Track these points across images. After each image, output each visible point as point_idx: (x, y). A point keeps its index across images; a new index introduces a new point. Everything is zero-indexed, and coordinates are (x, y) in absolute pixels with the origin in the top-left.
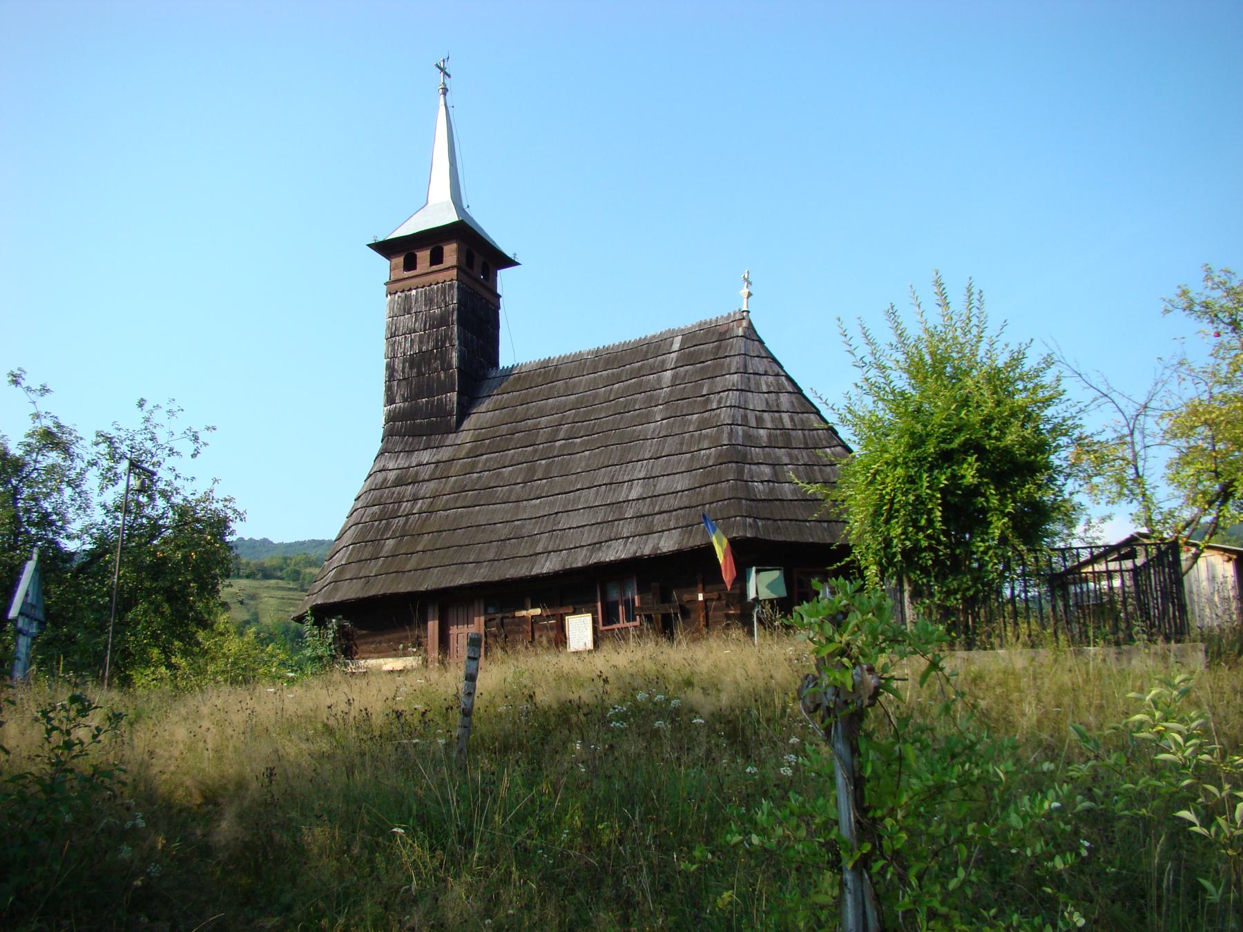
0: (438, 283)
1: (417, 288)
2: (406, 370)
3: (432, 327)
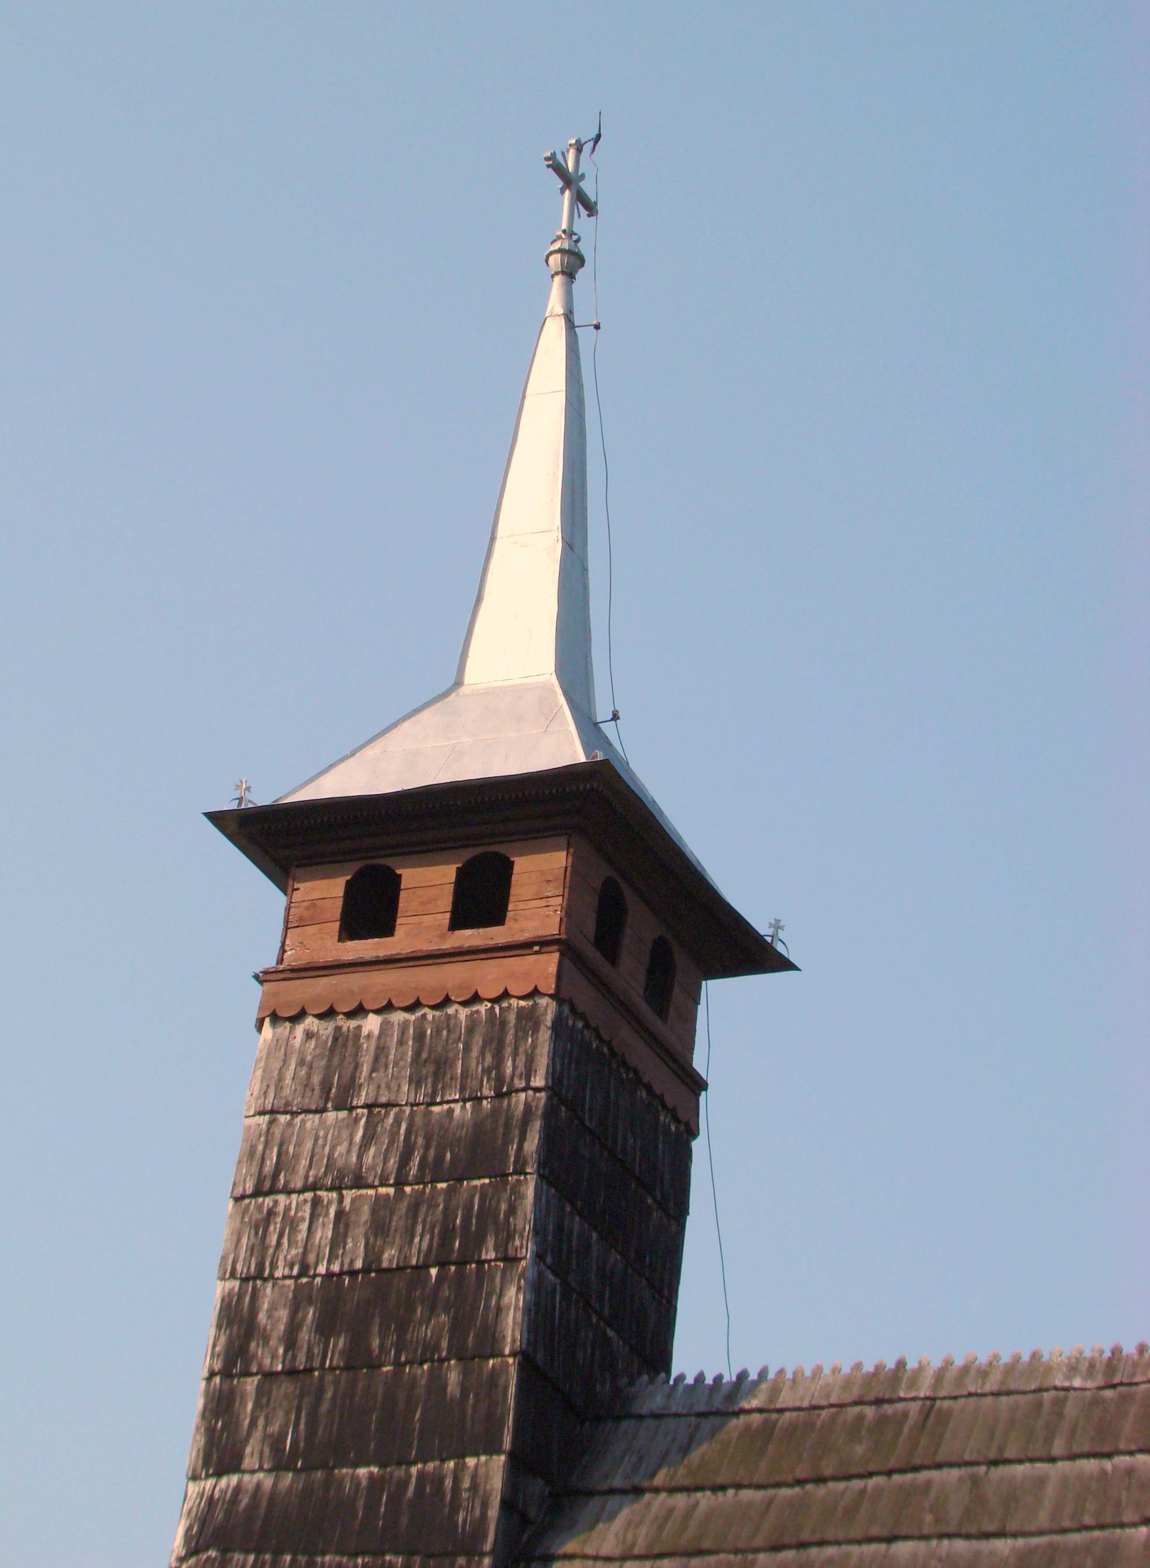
0: (476, 999)
1: (389, 1007)
2: (305, 1336)
3: (433, 1171)
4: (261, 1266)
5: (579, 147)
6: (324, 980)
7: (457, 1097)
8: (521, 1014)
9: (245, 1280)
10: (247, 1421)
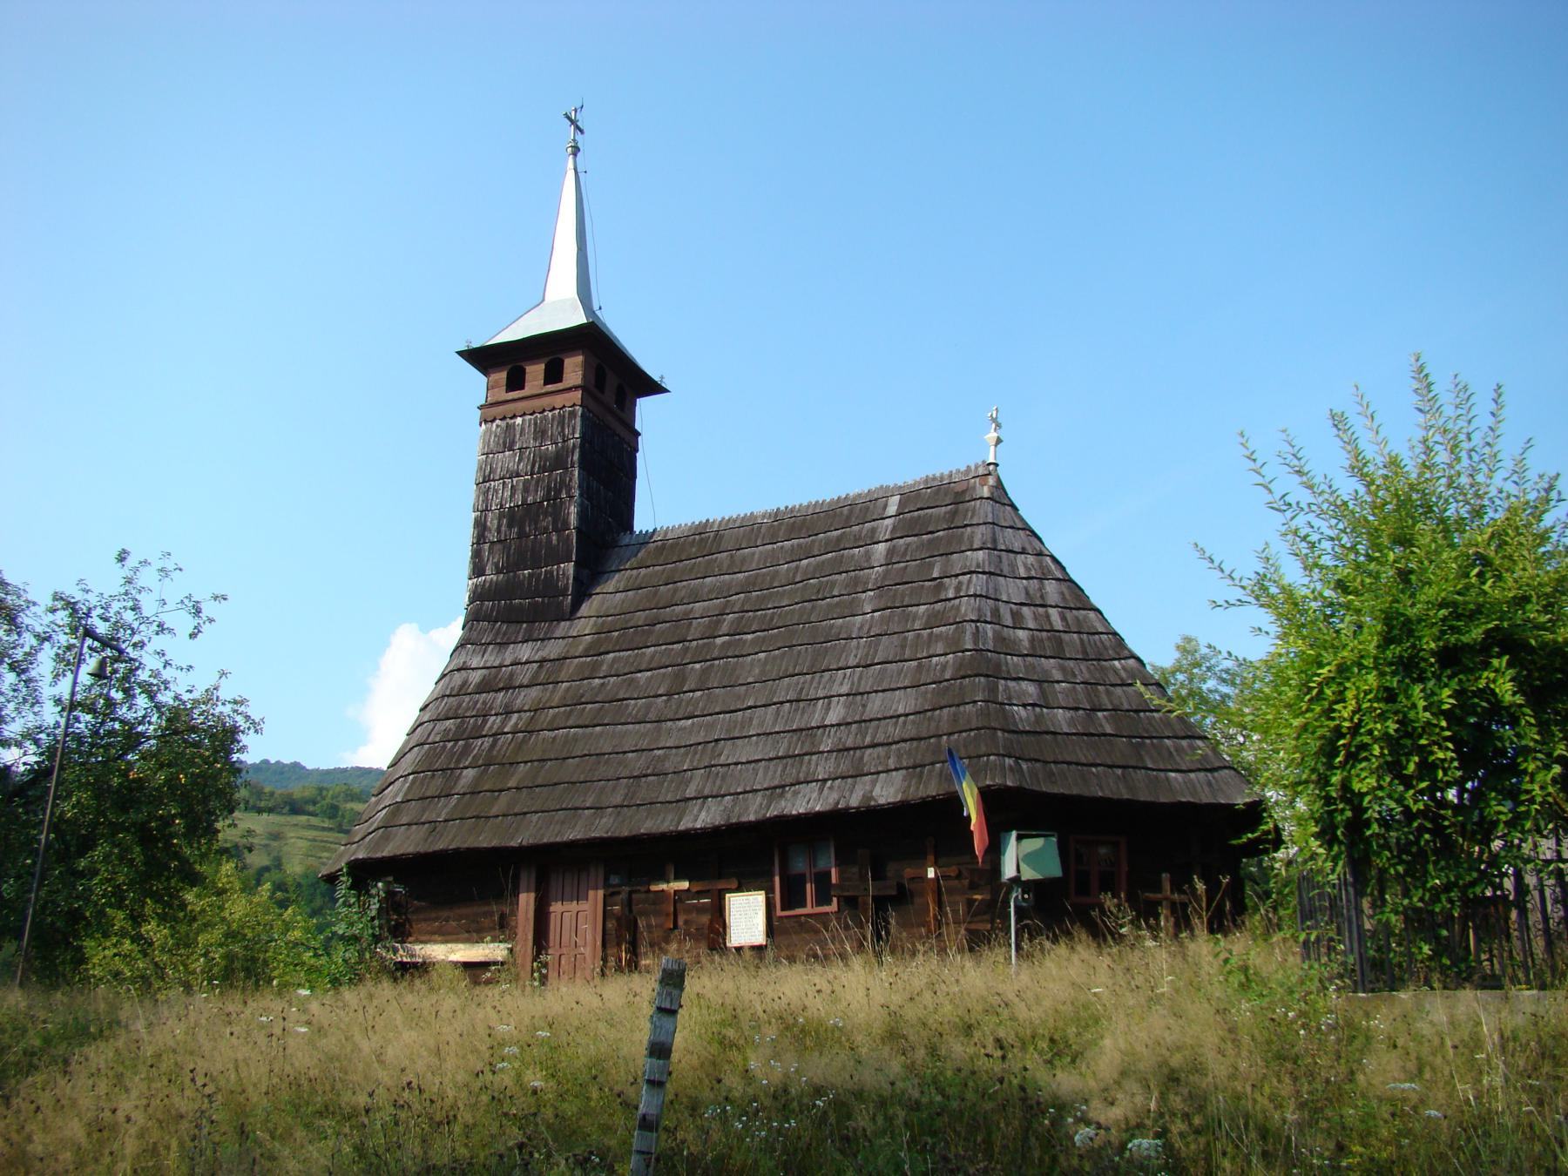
0: (554, 409)
1: (524, 414)
2: (503, 528)
3: (543, 469)
5: (576, 110)
8: (570, 412)
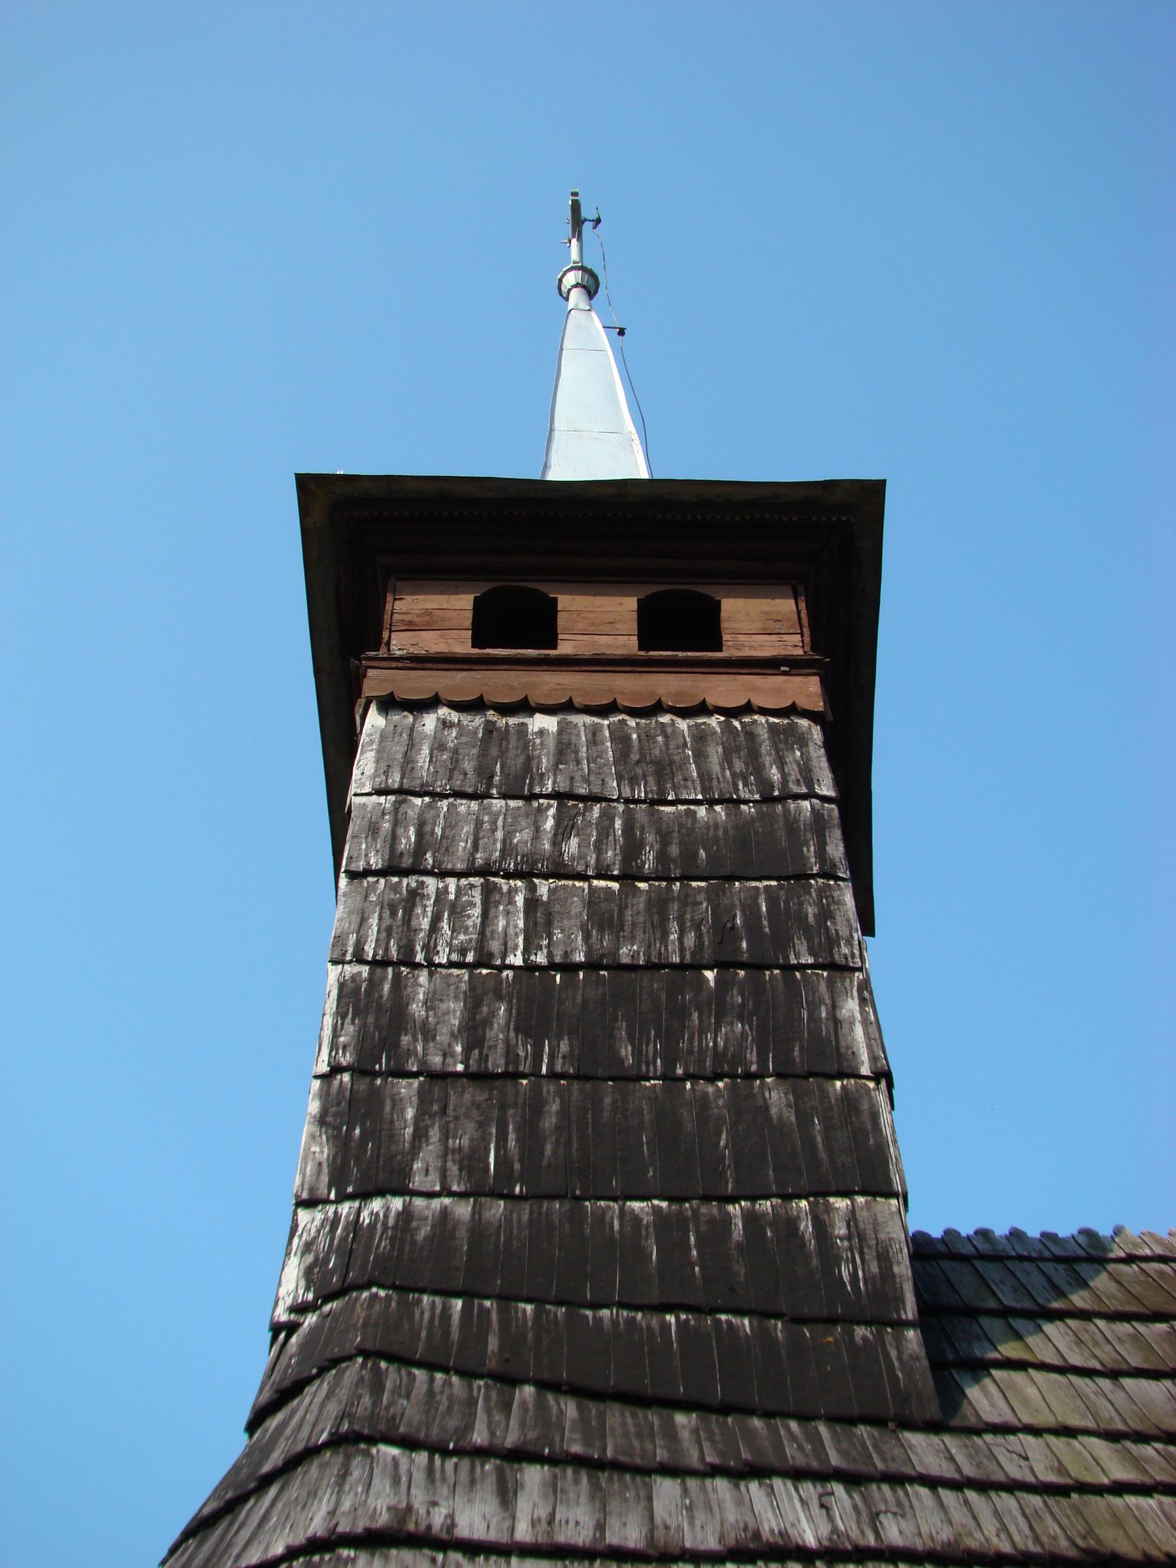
4: (407, 950)
6: (461, 675)
7: (700, 797)
9: (377, 964)
10: (409, 1131)
